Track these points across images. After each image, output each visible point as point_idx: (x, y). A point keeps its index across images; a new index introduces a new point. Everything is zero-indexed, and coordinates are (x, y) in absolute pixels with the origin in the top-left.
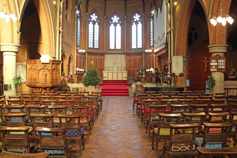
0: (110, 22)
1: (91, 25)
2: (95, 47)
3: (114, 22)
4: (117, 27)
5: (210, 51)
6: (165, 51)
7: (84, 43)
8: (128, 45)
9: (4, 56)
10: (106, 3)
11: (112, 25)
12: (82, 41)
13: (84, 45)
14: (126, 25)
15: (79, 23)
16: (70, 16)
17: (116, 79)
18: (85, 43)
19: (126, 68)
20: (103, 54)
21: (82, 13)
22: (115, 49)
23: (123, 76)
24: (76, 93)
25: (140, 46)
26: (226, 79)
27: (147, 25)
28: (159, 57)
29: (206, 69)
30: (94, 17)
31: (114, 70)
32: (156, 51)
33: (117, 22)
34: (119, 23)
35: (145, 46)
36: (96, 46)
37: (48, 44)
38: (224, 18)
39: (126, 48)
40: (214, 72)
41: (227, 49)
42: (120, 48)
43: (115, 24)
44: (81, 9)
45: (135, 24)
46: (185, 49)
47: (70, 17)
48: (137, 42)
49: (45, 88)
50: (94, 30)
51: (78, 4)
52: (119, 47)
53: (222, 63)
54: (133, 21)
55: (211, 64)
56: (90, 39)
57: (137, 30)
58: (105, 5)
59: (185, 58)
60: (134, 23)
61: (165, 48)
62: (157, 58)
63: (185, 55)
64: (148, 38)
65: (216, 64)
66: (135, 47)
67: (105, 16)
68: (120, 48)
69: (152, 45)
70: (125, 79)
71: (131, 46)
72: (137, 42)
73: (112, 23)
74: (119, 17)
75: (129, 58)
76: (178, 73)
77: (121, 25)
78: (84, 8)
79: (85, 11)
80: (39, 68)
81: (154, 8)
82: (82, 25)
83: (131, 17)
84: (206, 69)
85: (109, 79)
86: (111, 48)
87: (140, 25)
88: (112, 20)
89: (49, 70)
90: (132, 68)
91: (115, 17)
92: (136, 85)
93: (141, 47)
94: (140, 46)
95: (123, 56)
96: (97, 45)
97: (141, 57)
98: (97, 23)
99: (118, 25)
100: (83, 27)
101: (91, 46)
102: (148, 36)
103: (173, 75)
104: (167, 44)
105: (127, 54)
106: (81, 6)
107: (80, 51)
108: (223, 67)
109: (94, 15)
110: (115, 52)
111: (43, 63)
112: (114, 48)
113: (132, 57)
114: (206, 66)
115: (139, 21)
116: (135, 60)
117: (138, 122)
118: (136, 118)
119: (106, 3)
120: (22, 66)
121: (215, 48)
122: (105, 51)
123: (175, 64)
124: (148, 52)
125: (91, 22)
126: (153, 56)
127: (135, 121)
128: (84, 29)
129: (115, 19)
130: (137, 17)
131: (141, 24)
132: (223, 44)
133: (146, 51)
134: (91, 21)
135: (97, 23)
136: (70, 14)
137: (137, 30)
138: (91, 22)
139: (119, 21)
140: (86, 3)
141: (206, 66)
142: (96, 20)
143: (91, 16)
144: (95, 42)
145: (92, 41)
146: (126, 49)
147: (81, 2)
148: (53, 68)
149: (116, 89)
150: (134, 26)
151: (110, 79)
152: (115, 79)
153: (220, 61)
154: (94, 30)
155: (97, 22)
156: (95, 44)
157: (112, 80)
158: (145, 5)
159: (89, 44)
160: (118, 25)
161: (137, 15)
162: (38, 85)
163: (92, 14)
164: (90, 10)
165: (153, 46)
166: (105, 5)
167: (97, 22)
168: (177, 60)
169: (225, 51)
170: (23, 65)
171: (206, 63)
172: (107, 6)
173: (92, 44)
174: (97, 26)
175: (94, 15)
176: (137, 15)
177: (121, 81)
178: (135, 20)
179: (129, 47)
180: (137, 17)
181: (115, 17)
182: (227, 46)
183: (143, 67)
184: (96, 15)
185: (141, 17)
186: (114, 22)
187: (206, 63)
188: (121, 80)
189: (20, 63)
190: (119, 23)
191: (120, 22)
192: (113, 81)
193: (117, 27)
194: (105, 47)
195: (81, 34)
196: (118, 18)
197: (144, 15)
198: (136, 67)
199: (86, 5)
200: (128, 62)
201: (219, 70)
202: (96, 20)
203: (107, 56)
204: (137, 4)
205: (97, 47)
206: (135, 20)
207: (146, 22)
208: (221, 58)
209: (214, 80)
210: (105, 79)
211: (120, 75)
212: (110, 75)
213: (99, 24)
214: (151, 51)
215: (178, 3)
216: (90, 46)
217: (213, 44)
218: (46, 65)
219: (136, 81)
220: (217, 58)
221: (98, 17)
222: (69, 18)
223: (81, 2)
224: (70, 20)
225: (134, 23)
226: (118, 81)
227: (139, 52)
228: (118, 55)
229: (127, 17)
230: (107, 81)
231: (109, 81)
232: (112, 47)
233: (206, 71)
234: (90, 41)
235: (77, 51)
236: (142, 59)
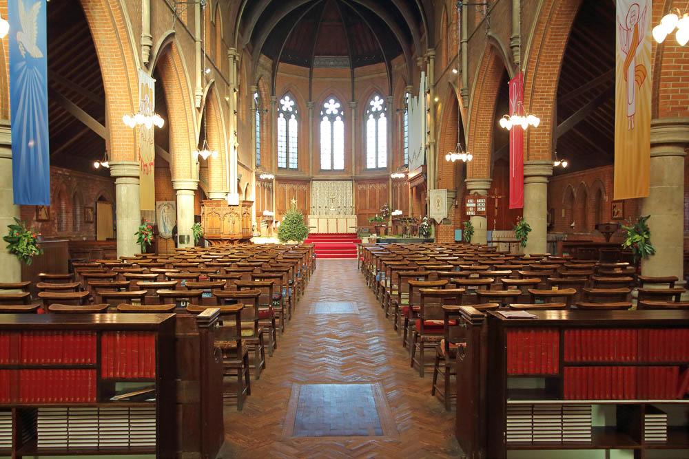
0: (322, 113)
1: (281, 121)
2: (291, 166)
3: (328, 112)
4: (335, 123)
5: (469, 187)
6: (421, 180)
7: (269, 160)
8: (358, 162)
9: (117, 186)
10: (311, 72)
11: (325, 118)
12: (265, 154)
13: (269, 164)
14: (355, 119)
15: (258, 117)
16: (244, 109)
17: (335, 232)
18: (271, 158)
19: (354, 209)
20: (307, 182)
21: (263, 96)
22: (332, 171)
23: (348, 225)
24: (199, 296)
25: (383, 164)
26: (490, 228)
27: (397, 122)
28: (417, 187)
29: (496, 211)
30: (287, 103)
31: (331, 213)
32: (411, 175)
33: (336, 112)
34: (339, 114)
35: (393, 164)
36: (293, 164)
37: (220, 171)
38: (524, 117)
39: (354, 167)
40: (473, 216)
41: (491, 185)
42: (342, 167)
43: (332, 118)
44: (262, 89)
45: (374, 117)
46: (452, 179)
47: (244, 112)
48: (377, 155)
49: (232, 241)
50: (288, 129)
51: (256, 80)
52: (340, 165)
53: (482, 204)
54: (368, 112)
55: (468, 205)
56: (279, 149)
57: (377, 130)
58: (311, 77)
59: (452, 193)
60: (371, 116)
61: (422, 173)
62: (414, 189)
63: (452, 188)
64: (400, 148)
65: (474, 205)
66: (373, 166)
67: (310, 101)
68: (342, 167)
69: (406, 162)
70: (353, 231)
71: (366, 164)
72: (377, 155)
73: (325, 114)
74: (341, 102)
75: (360, 187)
76: (439, 219)
77: (343, 118)
78: (267, 87)
79: (269, 92)
80: (224, 213)
81: (409, 90)
82: (265, 122)
83: (364, 103)
84: (496, 211)
85: (321, 232)
86: (323, 167)
87: (383, 120)
88: (324, 110)
89: (238, 215)
90: (366, 209)
91: (332, 101)
92: (369, 239)
93: (385, 165)
94: (383, 164)
95: (349, 184)
96: (296, 161)
97: (385, 186)
98: (293, 116)
99: (338, 118)
100: (267, 128)
101: (282, 164)
102: (400, 143)
103: (433, 221)
104: (425, 166)
105: (358, 181)
106: (261, 83)
107: (263, 177)
108: (484, 209)
109: (287, 98)
110: (331, 176)
111: (230, 206)
112: (285, 166)
113: (368, 187)
114: (496, 205)
115: (381, 112)
116: (373, 193)
117: (361, 278)
118: (360, 274)
119: (311, 72)
120: (169, 207)
121: (473, 183)
122: (311, 175)
123: (435, 202)
124: (397, 179)
125: (281, 115)
126: (407, 186)
127: (401, 407)
128: (269, 130)
129: (332, 106)
130: (377, 103)
131: (385, 119)
132: (483, 177)
133: (394, 176)
134: (281, 111)
135: (293, 116)
136: (244, 106)
137: (377, 130)
138: (281, 115)
139: (340, 110)
140: (270, 75)
141: (496, 205)
142: (291, 109)
143: (282, 102)
144: (291, 155)
145: (284, 155)
146: (355, 169)
147: (261, 76)
148: (244, 212)
149: (338, 245)
150: (371, 122)
151: (323, 230)
152: (333, 230)
153: (479, 201)
154: (288, 129)
155: (293, 112)
156: (291, 160)
157: (326, 232)
158: (394, 79)
159: (279, 160)
160: (338, 118)
161: (377, 98)
162: (223, 237)
163: (283, 97)
164: (279, 89)
165: (407, 166)
166: (311, 77)
167: (293, 112)
168: (438, 196)
169: (488, 187)
170: (170, 207)
171: (496, 200)
172: (313, 80)
173: (284, 160)
174: (293, 123)
175: (287, 98)
176: (377, 98)
177: (343, 234)
178: (374, 110)
179: (360, 165)
180: (377, 103)
181: (332, 101)
182: (491, 180)
183: (388, 207)
184: (291, 99)
185: (385, 102)
186: (328, 112)
187: (496, 200)
188: (345, 232)
189: (165, 203)
190: (339, 114)
191: (342, 113)
192: (328, 234)
193: (290, 120)
194: (311, 167)
195: (263, 140)
196: (338, 105)
197: (390, 100)
198: (375, 207)
199: (271, 79)
200: (360, 195)
201: (478, 213)
202: (291, 109)
203: (316, 185)
204: (377, 75)
205: (295, 166)
206: (374, 110)
207: (395, 114)
208: (480, 197)
209: (472, 227)
210: (313, 231)
211: (342, 222)
212: (323, 222)
213: (298, 117)
214: (402, 176)
215: (440, 97)
216: (280, 165)
217: (470, 178)
218: (235, 207)
219: (371, 232)
220: (476, 197)
221: (296, 102)
222: (242, 114)
223: (261, 76)
224: (244, 117)
225: (371, 116)
226: (338, 234)
227: (381, 177)
228: (339, 182)
229: (357, 103)
230: (317, 234)
231: (320, 234)
232: (325, 165)
233: (496, 214)
234: (279, 154)
235: (257, 177)
236: (386, 191)
